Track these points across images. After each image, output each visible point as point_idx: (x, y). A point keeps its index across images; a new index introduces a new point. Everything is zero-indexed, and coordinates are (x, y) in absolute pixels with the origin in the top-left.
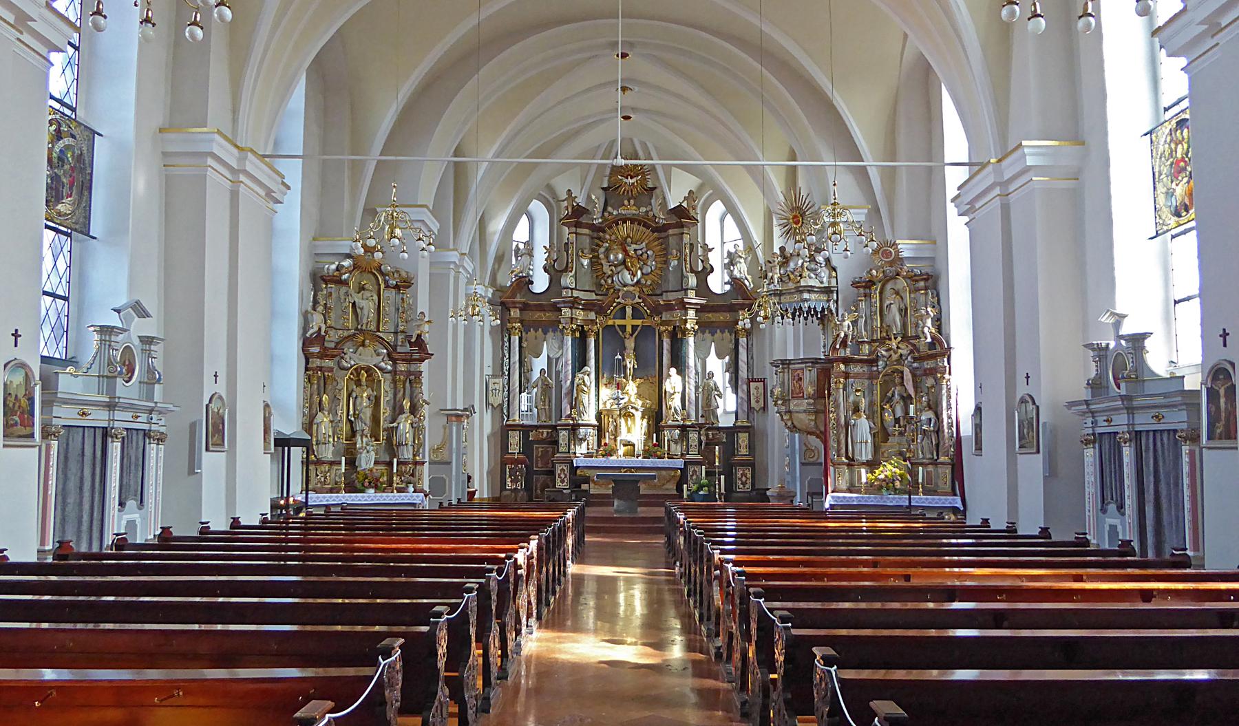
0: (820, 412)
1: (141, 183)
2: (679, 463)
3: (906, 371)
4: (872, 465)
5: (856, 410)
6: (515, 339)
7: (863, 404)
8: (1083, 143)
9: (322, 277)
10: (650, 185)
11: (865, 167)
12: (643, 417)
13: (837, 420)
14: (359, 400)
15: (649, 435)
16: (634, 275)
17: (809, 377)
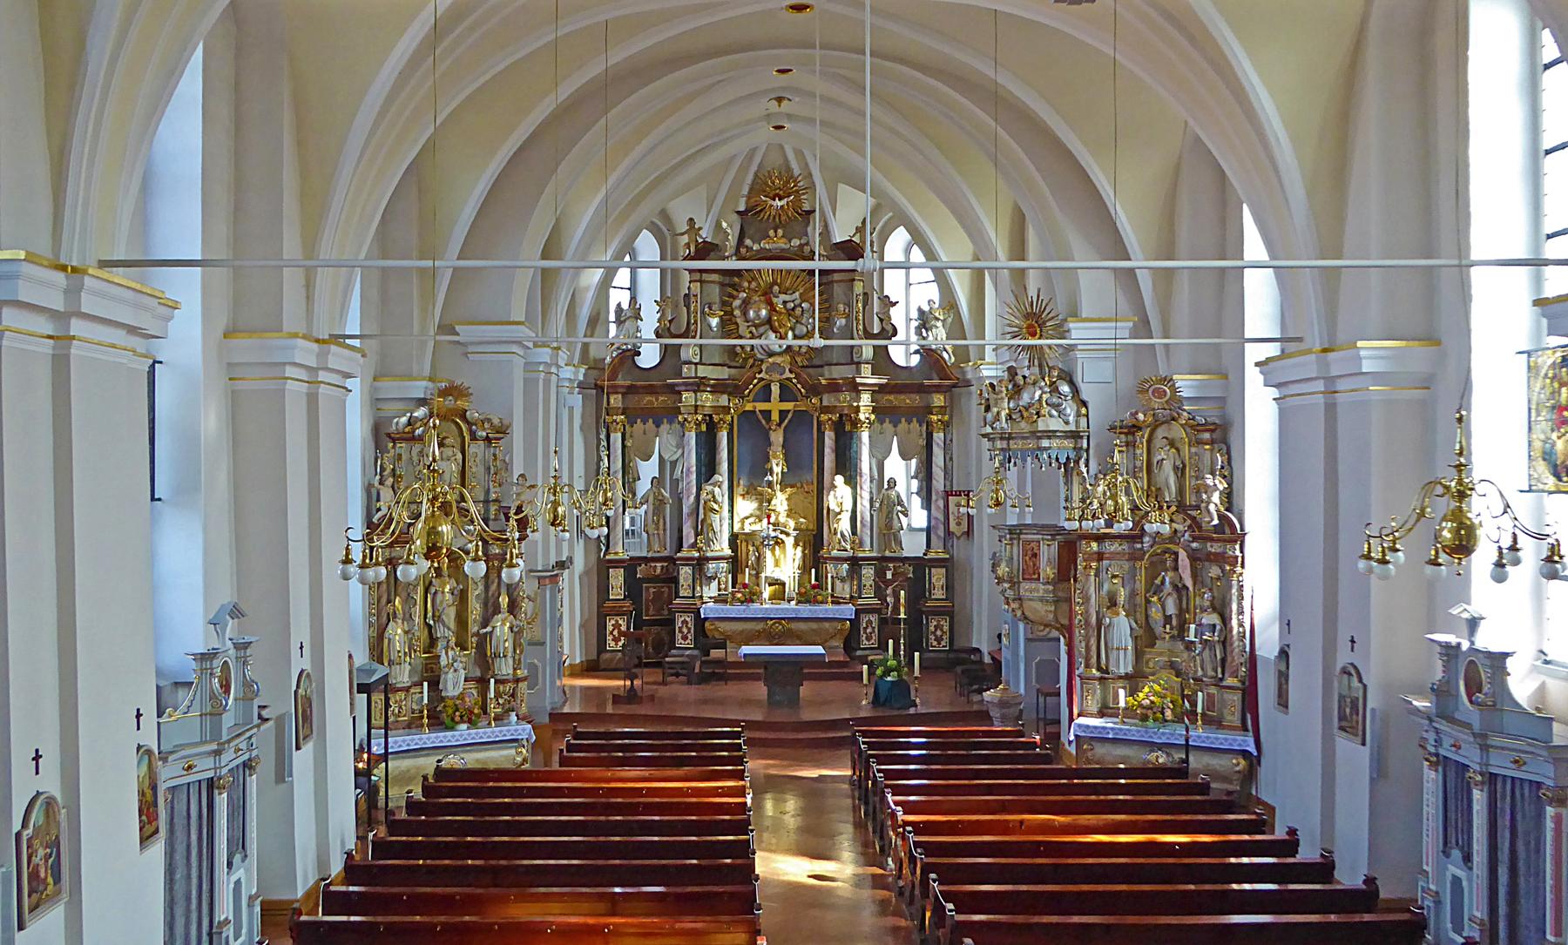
0: (1063, 601)
1: (211, 422)
2: (848, 611)
3: (1182, 555)
4: (1134, 681)
5: (1113, 603)
6: (617, 438)
7: (1122, 596)
8: (1438, 343)
9: (389, 435)
10: (806, 207)
11: (1132, 271)
12: (796, 544)
13: (1086, 614)
14: (439, 597)
17: (1048, 552)
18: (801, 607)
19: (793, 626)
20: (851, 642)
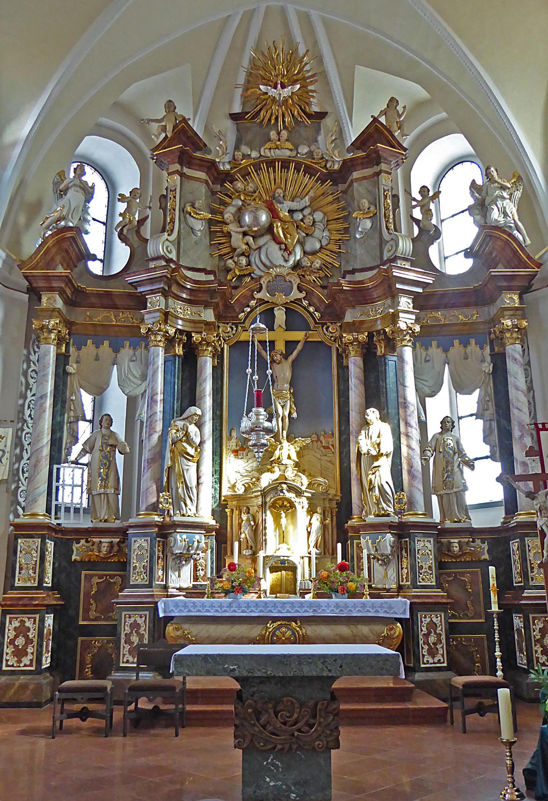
2: (400, 607)
12: (311, 511)
15: (325, 549)
16: (287, 250)
20: (408, 645)
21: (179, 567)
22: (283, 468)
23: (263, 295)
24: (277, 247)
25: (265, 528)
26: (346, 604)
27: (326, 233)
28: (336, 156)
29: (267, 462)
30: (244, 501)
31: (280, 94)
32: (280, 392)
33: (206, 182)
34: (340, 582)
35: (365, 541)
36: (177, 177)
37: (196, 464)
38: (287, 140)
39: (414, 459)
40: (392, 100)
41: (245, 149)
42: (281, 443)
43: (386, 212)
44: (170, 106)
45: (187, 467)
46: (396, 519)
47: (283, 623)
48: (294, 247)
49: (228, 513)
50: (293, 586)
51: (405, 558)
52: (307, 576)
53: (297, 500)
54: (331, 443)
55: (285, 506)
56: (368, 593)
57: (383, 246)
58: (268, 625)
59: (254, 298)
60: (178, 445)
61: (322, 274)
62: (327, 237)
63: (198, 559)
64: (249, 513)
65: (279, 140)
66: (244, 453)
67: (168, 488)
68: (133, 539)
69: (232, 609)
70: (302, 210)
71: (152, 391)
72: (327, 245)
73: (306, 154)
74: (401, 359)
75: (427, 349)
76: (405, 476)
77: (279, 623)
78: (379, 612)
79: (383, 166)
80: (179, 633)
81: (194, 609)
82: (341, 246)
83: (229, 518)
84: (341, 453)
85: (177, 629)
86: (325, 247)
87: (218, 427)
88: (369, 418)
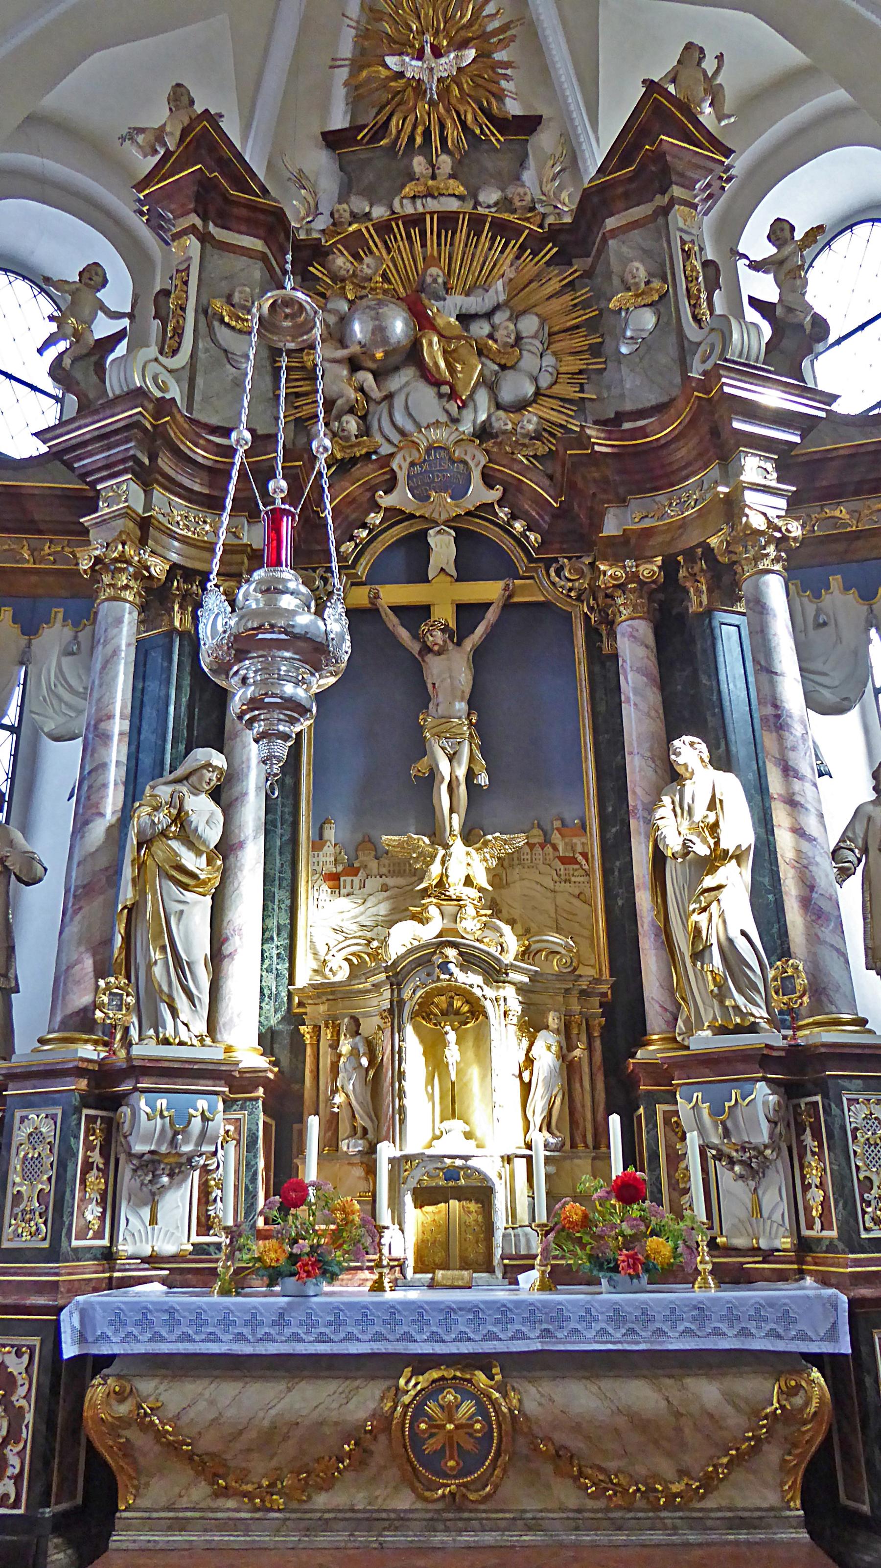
12: (531, 1026)
15: (574, 1132)
18: (568, 1297)
19: (533, 1398)
21: (153, 1194)
22: (450, 908)
23: (400, 498)
24: (429, 392)
25: (401, 1076)
26: (644, 1312)
27: (549, 360)
28: (564, 204)
29: (409, 890)
30: (347, 1003)
31: (431, 70)
32: (444, 720)
33: (264, 258)
34: (624, 1236)
35: (690, 1106)
36: (192, 244)
37: (208, 900)
38: (451, 176)
39: (817, 864)
40: (689, 46)
41: (360, 205)
42: (447, 847)
43: (690, 285)
44: (179, 96)
45: (180, 907)
46: (776, 1039)
47: (449, 1373)
48: (473, 392)
49: (308, 1036)
50: (481, 1248)
51: (814, 1154)
52: (523, 1215)
53: (490, 992)
54: (579, 849)
55: (457, 1013)
56: (709, 1267)
57: (688, 361)
58: (402, 1382)
59: (377, 507)
60: (159, 850)
61: (541, 449)
62: (550, 369)
63: (214, 1166)
64: (357, 1033)
65: (434, 177)
66: (356, 880)
67: (128, 967)
68: (18, 1114)
69: (288, 1331)
70: (488, 315)
71: (98, 710)
72: (550, 387)
73: (496, 204)
74: (759, 608)
75: (818, 596)
76: (794, 916)
77: (435, 1374)
78: (752, 1335)
79: (677, 191)
80: (123, 1409)
81: (172, 1331)
82: (586, 386)
83: (309, 1051)
84: (606, 872)
85: (121, 1396)
86: (547, 392)
87: (287, 816)
88: (681, 760)
